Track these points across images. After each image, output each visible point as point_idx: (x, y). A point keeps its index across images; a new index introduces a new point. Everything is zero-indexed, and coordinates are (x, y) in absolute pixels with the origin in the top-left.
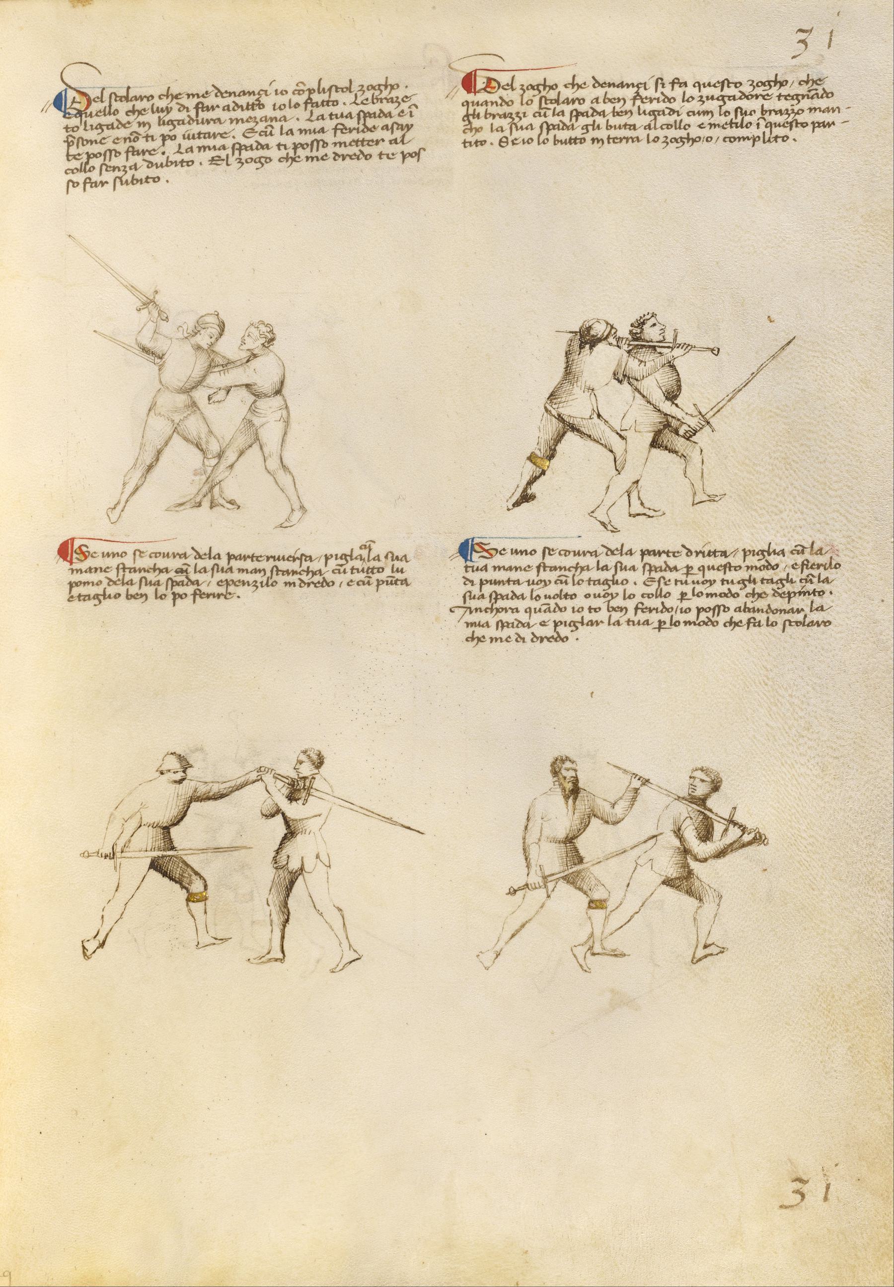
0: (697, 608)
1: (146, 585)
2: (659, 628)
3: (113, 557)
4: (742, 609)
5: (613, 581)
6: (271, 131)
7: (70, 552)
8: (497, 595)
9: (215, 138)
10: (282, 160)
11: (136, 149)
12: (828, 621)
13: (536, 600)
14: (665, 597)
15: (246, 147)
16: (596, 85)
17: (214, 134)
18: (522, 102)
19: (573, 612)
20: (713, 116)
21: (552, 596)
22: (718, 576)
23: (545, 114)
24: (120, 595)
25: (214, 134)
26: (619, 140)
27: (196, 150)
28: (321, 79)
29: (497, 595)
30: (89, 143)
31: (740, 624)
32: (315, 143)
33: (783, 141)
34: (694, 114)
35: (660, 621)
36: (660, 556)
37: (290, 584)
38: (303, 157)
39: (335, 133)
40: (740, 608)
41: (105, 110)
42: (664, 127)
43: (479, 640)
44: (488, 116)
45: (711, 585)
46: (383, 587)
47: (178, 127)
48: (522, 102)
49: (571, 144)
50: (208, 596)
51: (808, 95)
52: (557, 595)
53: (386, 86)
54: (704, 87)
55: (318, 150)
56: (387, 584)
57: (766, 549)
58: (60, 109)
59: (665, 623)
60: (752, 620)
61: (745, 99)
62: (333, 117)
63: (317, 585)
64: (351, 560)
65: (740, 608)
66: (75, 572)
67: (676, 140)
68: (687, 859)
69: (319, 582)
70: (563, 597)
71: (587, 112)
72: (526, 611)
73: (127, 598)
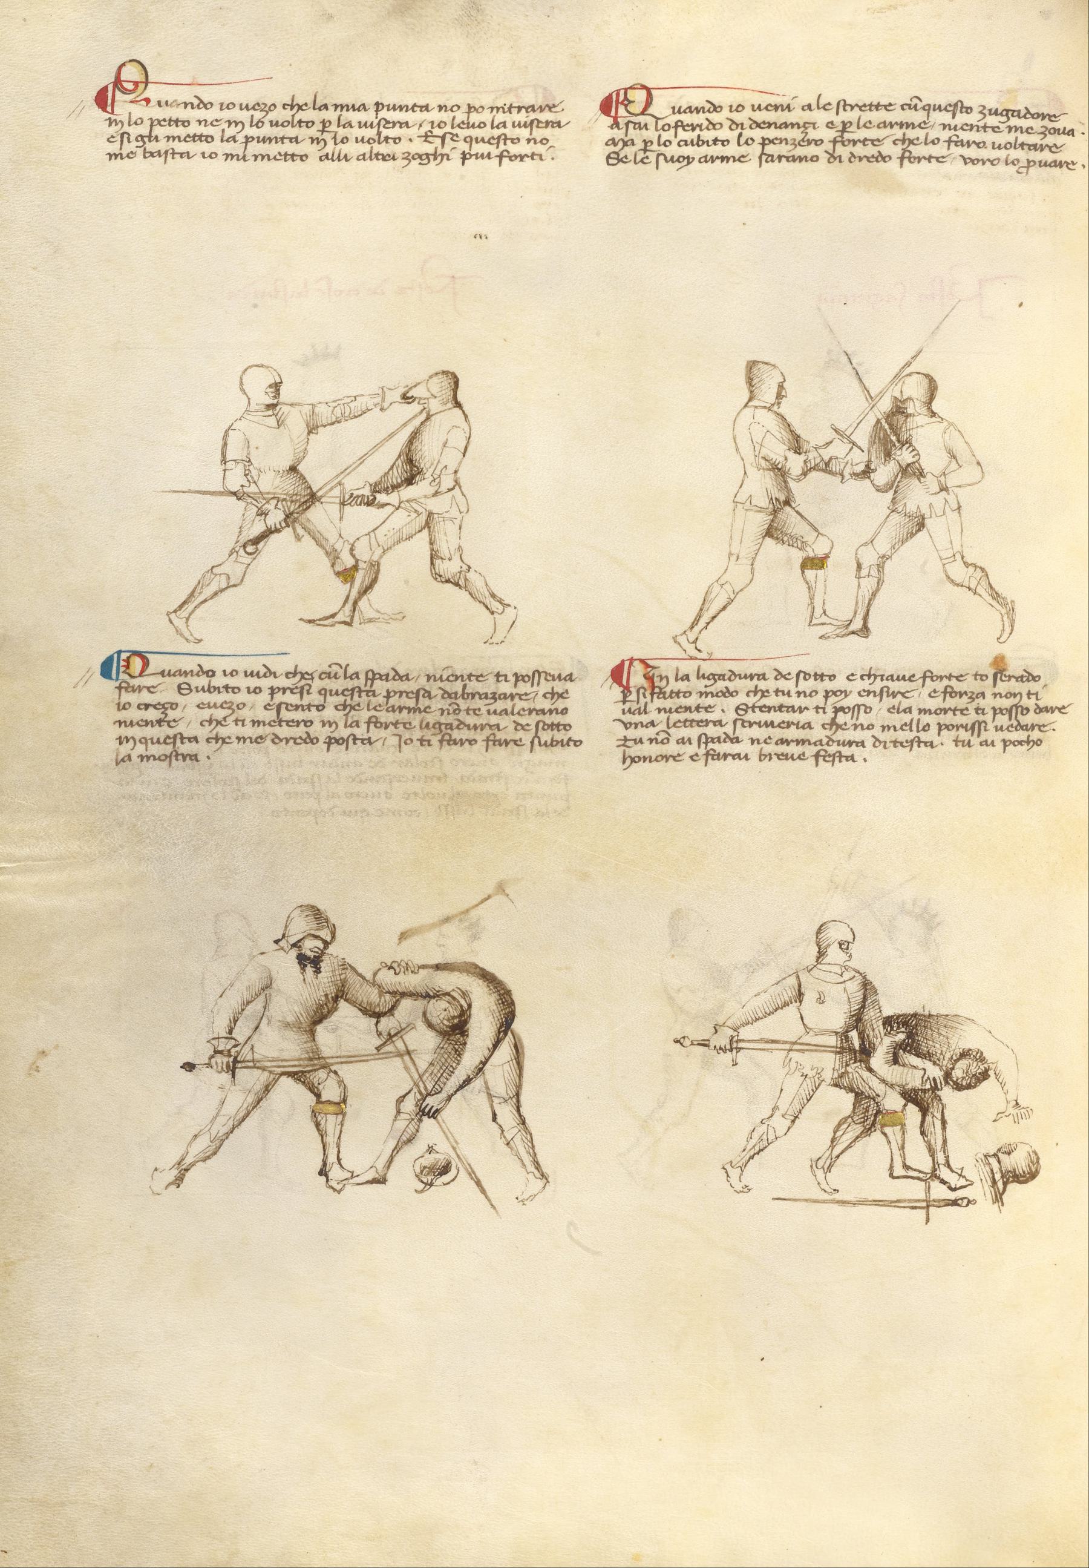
3: (800, 161)
4: (695, 142)
7: (109, 101)
8: (374, 675)
9: (969, 146)
10: (204, 723)
11: (453, 738)
13: (258, 127)
15: (203, 689)
17: (968, 142)
19: (271, 126)
20: (135, 744)
22: (524, 133)
23: (916, 106)
25: (968, 142)
26: (785, 725)
27: (976, 110)
28: (820, 95)
30: (519, 159)
32: (536, 675)
33: (395, 143)
34: (686, 145)
35: (323, 122)
39: (949, 145)
42: (905, 107)
44: (763, 757)
45: (689, 163)
47: (1011, 118)
50: (919, 159)
51: (656, 739)
54: (477, 142)
55: (979, 736)
58: (104, 110)
60: (949, 690)
61: (783, 679)
63: (871, 160)
66: (113, 157)
69: (873, 156)
71: (387, 675)
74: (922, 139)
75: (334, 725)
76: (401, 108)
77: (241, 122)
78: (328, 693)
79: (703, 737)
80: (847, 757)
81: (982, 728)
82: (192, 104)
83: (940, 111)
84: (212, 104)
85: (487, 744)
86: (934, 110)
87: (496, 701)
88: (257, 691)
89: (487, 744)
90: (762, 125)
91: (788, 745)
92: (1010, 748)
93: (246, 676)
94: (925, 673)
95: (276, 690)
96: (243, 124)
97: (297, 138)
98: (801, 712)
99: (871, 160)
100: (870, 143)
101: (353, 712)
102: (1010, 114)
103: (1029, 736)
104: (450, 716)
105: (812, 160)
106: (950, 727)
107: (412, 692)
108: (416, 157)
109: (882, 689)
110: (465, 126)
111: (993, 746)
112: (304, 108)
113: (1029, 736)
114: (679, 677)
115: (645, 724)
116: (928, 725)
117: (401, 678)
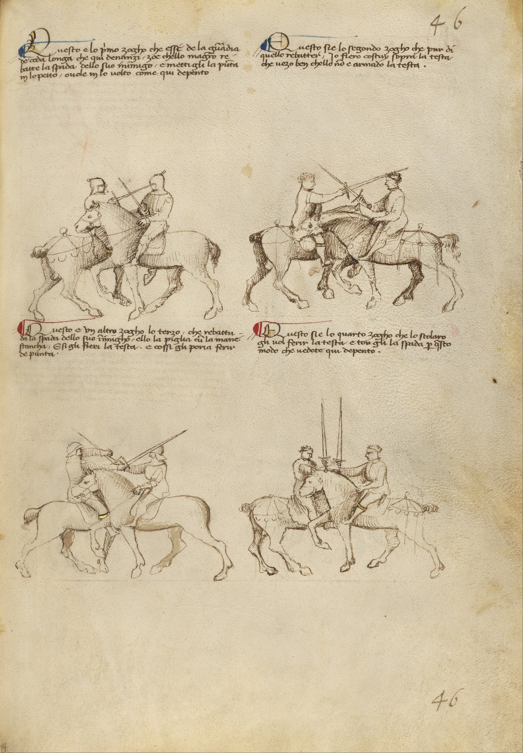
0: (30, 352)
1: (106, 67)
2: (428, 348)
5: (265, 342)
6: (201, 340)
8: (57, 66)
10: (313, 64)
12: (142, 331)
14: (76, 339)
16: (189, 49)
18: (411, 335)
21: (75, 74)
23: (201, 340)
24: (293, 64)
26: (353, 57)
29: (57, 66)
31: (271, 65)
36: (354, 336)
37: (94, 74)
38: (88, 73)
40: (101, 330)
41: (324, 63)
43: (269, 65)
46: (223, 68)
48: (411, 335)
49: (125, 75)
52: (120, 72)
53: (136, 331)
56: (225, 66)
57: (135, 329)
59: (431, 344)
60: (291, 341)
62: (360, 343)
64: (216, 50)
65: (101, 330)
67: (131, 50)
68: (350, 265)
70: (105, 331)
72: (261, 57)
73: (296, 66)
74: (41, 67)
75: (26, 78)
76: (363, 351)
77: (26, 76)
78: (166, 73)
79: (55, 66)
80: (415, 65)
81: (169, 348)
82: (370, 48)
83: (74, 76)
84: (307, 334)
85: (217, 349)
86: (97, 59)
87: (389, 52)
88: (67, 75)
89: (217, 349)
90: (301, 64)
91: (440, 51)
92: (34, 357)
93: (112, 75)
94: (289, 340)
95: (431, 50)
96: (97, 75)
97: (448, 57)
98: (440, 51)
99: (313, 56)
100: (35, 69)
101: (120, 71)
102: (67, 59)
103: (316, 60)
104: (175, 68)
105: (68, 74)
106: (363, 343)
107: (437, 56)
108: (392, 49)
109: (373, 55)
110: (306, 351)
111: (21, 77)
112: (271, 65)
113: (316, 60)
114: (156, 339)
115: (197, 56)
116: (86, 73)
117: (419, 345)
